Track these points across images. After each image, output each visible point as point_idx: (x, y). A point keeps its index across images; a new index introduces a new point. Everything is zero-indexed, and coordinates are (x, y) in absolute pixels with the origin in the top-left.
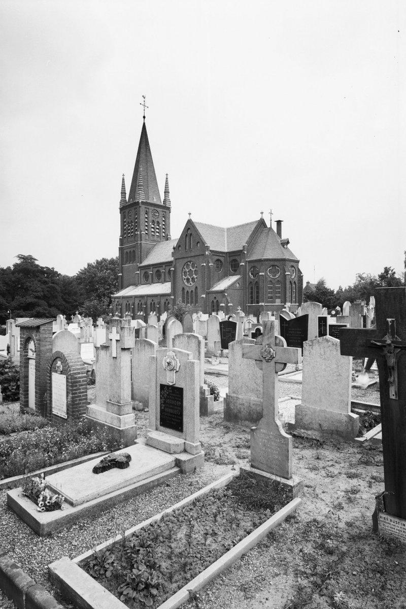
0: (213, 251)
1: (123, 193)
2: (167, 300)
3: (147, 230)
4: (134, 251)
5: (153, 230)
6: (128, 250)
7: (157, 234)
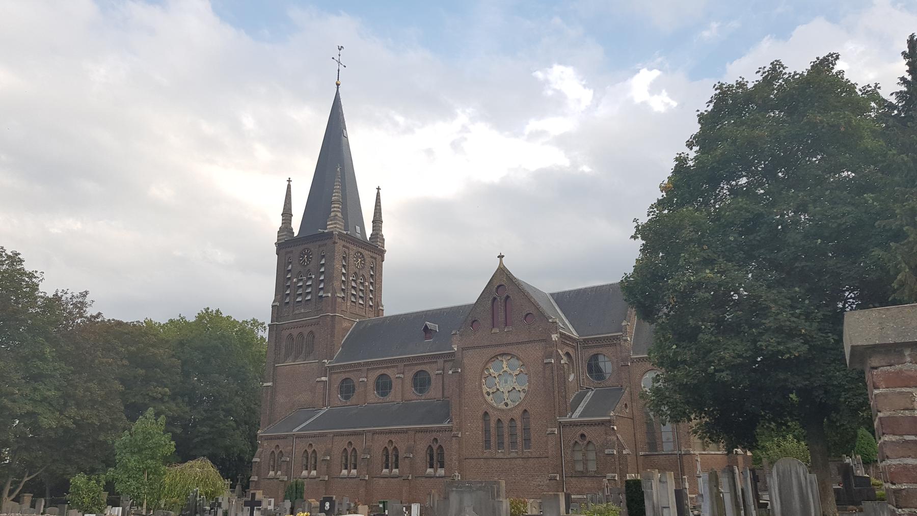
1: (287, 214)
4: (311, 332)
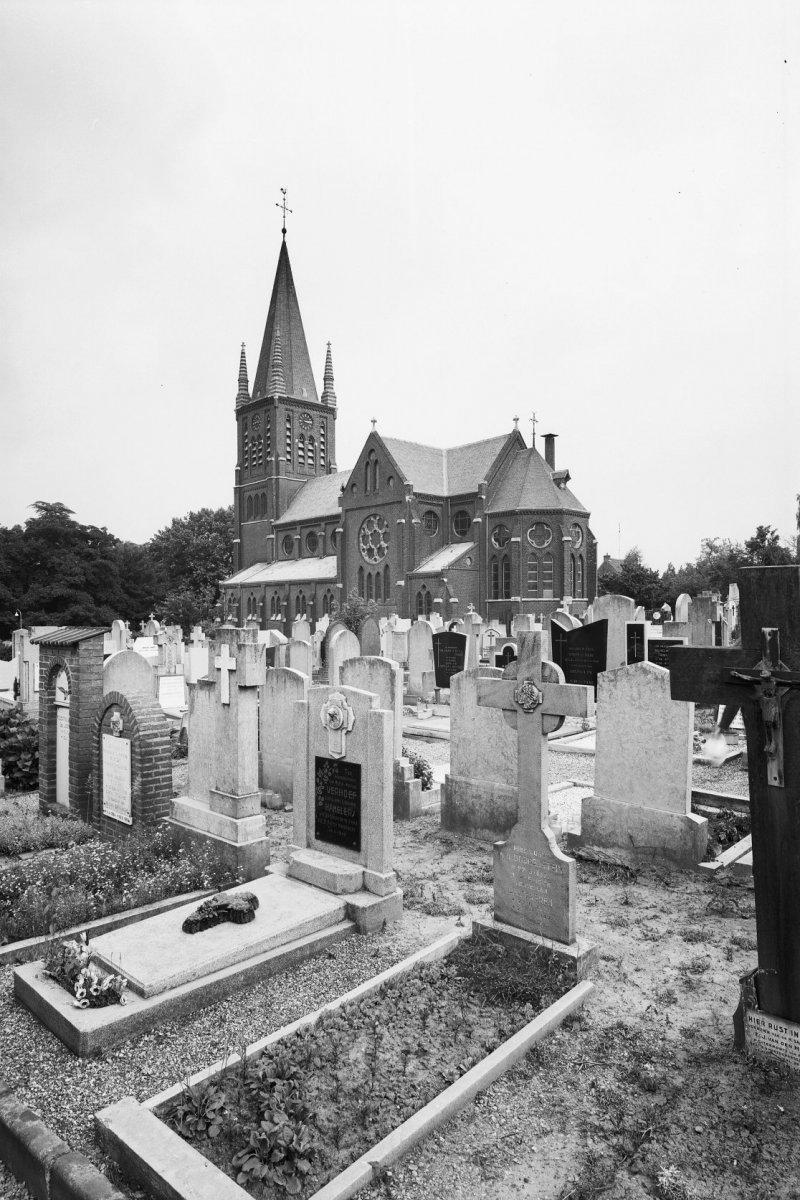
0: (420, 494)
1: (243, 380)
2: (329, 590)
3: (289, 453)
4: (264, 495)
5: (301, 453)
6: (253, 493)
7: (310, 461)
